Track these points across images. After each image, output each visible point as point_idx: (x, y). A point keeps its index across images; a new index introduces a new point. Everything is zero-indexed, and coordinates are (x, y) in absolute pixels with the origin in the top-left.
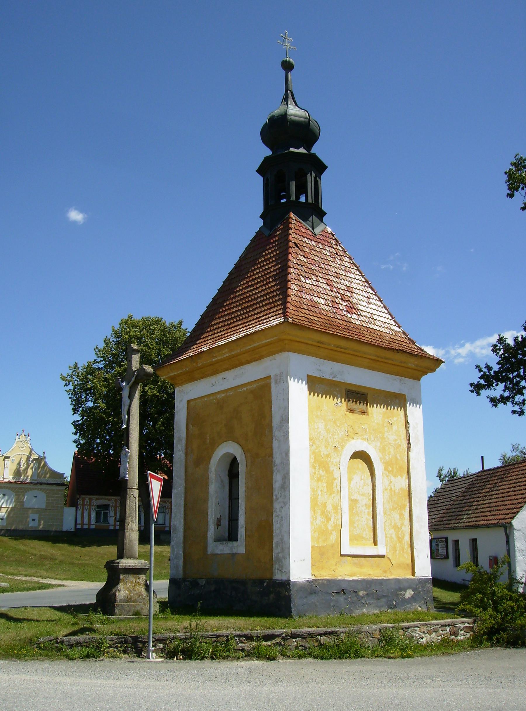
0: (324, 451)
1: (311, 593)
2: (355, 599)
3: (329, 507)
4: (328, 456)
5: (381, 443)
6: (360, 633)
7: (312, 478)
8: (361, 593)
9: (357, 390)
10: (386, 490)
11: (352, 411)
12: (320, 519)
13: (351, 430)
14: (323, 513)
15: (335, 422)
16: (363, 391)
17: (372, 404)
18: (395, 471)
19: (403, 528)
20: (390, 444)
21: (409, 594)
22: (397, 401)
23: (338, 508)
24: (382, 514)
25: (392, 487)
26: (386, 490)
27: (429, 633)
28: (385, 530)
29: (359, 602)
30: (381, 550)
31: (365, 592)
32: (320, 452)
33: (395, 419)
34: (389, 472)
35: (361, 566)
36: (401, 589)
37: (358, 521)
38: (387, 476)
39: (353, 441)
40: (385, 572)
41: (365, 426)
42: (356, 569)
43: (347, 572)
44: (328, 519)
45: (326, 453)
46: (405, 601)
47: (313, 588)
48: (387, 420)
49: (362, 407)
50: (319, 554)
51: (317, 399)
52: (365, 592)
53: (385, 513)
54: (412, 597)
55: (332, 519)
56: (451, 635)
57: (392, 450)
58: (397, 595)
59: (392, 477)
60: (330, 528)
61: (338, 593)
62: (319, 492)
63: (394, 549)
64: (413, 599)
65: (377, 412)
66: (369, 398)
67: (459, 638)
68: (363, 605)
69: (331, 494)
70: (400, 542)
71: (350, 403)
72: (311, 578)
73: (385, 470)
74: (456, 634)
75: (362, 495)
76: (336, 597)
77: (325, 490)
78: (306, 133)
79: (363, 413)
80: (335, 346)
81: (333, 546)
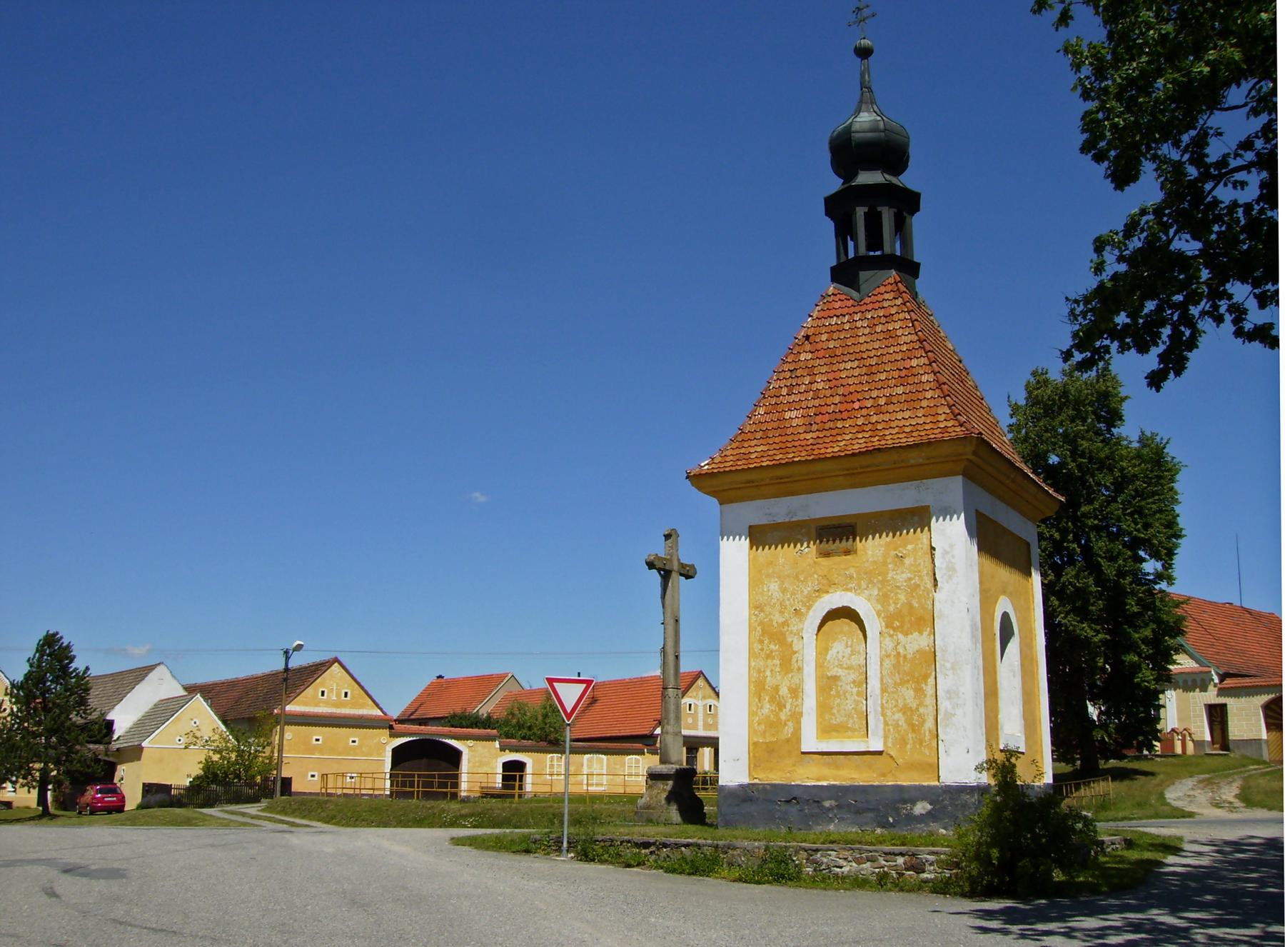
0: (778, 618)
1: (744, 801)
2: (817, 810)
3: (784, 691)
4: (785, 623)
5: (879, 590)
6: (735, 848)
7: (752, 654)
8: (827, 804)
9: (836, 522)
10: (888, 656)
11: (827, 554)
12: (767, 708)
13: (825, 581)
14: (772, 700)
15: (796, 577)
16: (848, 521)
17: (864, 536)
18: (907, 626)
19: (921, 710)
20: (898, 587)
21: (921, 808)
22: (916, 519)
23: (796, 692)
24: (878, 692)
25: (901, 650)
26: (888, 656)
27: (858, 861)
28: (883, 714)
29: (824, 815)
30: (875, 744)
31: (833, 803)
32: (771, 620)
33: (910, 547)
34: (894, 629)
35: (837, 767)
36: (905, 801)
37: (838, 705)
38: (891, 636)
39: (826, 597)
40: (884, 775)
41: (852, 570)
42: (826, 771)
43: (809, 776)
44: (781, 706)
45: (781, 620)
46: (912, 819)
47: (745, 795)
48: (893, 553)
49: (845, 544)
50: (761, 753)
51: (765, 554)
52: (833, 803)
53: (884, 690)
54: (929, 813)
55: (788, 706)
56: (907, 869)
57: (902, 597)
58: (897, 810)
59: (900, 636)
60: (783, 718)
61: (788, 802)
62: (768, 673)
63: (903, 742)
64: (930, 816)
65: (872, 548)
66: (858, 530)
67: (925, 875)
68: (831, 820)
69: (787, 673)
70: (914, 731)
71: (824, 545)
72: (745, 780)
73: (887, 627)
74: (919, 869)
75: (848, 668)
76: (784, 807)
77: (778, 669)
78: (889, 152)
79: (847, 552)
80: (771, 479)
81: (788, 741)
